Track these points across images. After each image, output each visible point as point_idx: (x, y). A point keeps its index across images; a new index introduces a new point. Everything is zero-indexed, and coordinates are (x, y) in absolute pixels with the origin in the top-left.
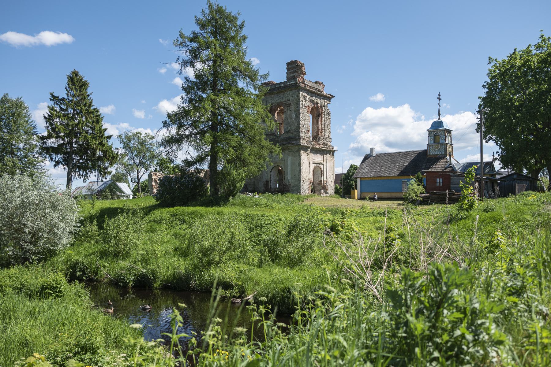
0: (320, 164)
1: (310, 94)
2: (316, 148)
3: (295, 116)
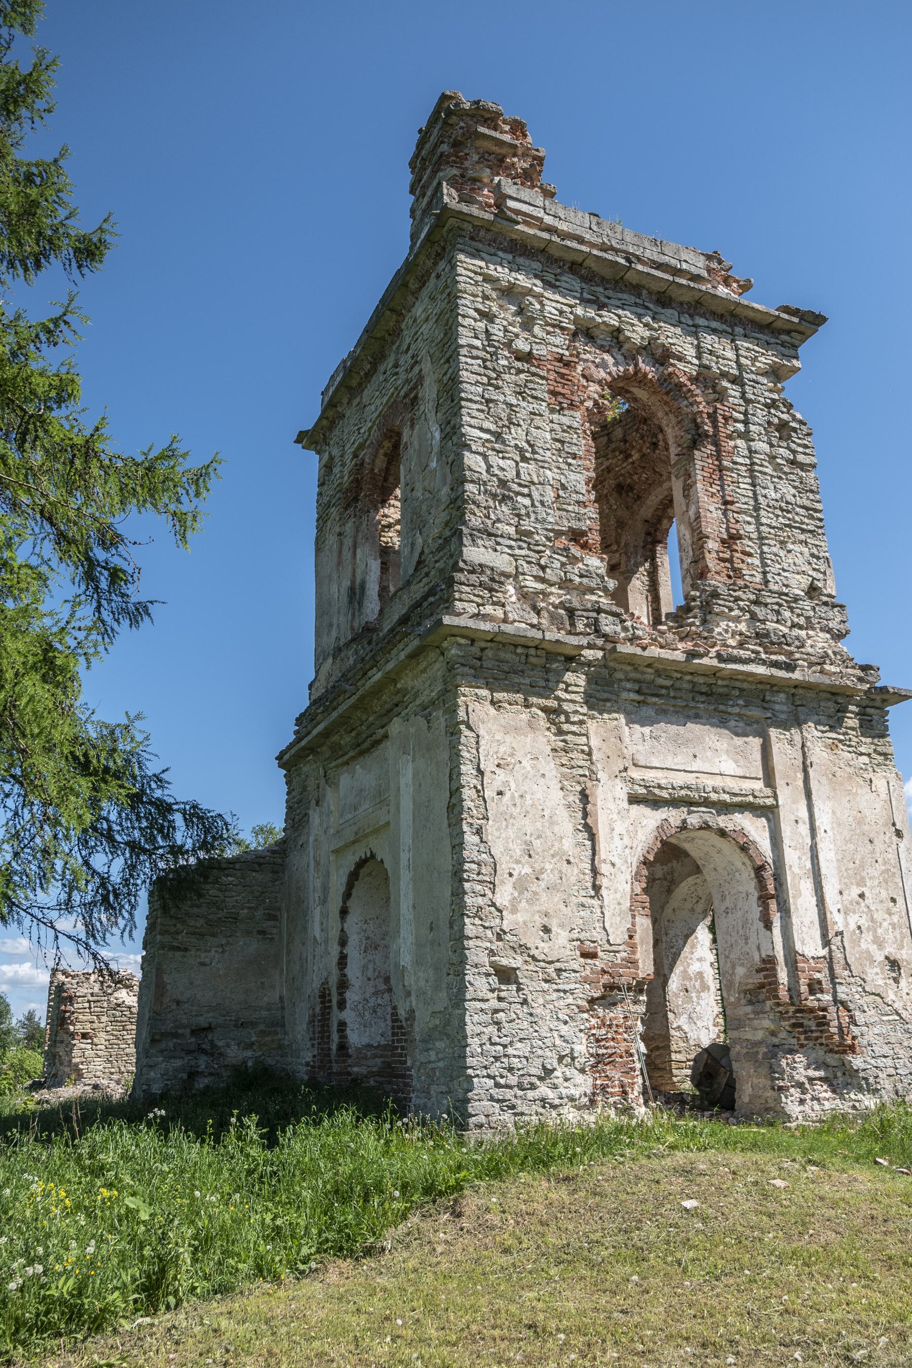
0: (725, 808)
1: (568, 280)
2: (659, 667)
3: (437, 435)
